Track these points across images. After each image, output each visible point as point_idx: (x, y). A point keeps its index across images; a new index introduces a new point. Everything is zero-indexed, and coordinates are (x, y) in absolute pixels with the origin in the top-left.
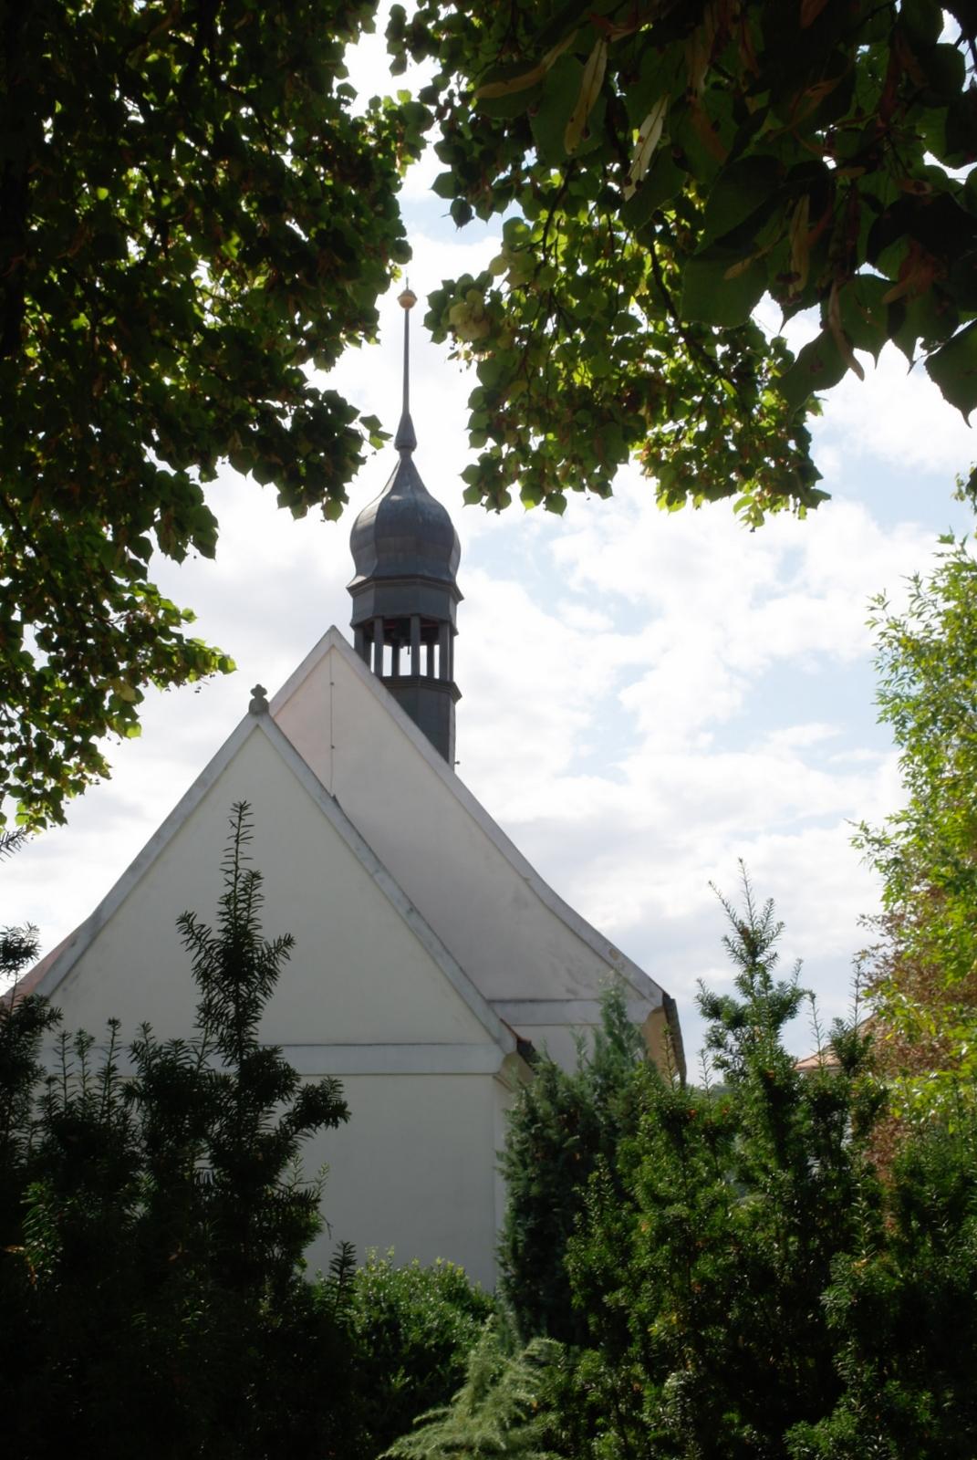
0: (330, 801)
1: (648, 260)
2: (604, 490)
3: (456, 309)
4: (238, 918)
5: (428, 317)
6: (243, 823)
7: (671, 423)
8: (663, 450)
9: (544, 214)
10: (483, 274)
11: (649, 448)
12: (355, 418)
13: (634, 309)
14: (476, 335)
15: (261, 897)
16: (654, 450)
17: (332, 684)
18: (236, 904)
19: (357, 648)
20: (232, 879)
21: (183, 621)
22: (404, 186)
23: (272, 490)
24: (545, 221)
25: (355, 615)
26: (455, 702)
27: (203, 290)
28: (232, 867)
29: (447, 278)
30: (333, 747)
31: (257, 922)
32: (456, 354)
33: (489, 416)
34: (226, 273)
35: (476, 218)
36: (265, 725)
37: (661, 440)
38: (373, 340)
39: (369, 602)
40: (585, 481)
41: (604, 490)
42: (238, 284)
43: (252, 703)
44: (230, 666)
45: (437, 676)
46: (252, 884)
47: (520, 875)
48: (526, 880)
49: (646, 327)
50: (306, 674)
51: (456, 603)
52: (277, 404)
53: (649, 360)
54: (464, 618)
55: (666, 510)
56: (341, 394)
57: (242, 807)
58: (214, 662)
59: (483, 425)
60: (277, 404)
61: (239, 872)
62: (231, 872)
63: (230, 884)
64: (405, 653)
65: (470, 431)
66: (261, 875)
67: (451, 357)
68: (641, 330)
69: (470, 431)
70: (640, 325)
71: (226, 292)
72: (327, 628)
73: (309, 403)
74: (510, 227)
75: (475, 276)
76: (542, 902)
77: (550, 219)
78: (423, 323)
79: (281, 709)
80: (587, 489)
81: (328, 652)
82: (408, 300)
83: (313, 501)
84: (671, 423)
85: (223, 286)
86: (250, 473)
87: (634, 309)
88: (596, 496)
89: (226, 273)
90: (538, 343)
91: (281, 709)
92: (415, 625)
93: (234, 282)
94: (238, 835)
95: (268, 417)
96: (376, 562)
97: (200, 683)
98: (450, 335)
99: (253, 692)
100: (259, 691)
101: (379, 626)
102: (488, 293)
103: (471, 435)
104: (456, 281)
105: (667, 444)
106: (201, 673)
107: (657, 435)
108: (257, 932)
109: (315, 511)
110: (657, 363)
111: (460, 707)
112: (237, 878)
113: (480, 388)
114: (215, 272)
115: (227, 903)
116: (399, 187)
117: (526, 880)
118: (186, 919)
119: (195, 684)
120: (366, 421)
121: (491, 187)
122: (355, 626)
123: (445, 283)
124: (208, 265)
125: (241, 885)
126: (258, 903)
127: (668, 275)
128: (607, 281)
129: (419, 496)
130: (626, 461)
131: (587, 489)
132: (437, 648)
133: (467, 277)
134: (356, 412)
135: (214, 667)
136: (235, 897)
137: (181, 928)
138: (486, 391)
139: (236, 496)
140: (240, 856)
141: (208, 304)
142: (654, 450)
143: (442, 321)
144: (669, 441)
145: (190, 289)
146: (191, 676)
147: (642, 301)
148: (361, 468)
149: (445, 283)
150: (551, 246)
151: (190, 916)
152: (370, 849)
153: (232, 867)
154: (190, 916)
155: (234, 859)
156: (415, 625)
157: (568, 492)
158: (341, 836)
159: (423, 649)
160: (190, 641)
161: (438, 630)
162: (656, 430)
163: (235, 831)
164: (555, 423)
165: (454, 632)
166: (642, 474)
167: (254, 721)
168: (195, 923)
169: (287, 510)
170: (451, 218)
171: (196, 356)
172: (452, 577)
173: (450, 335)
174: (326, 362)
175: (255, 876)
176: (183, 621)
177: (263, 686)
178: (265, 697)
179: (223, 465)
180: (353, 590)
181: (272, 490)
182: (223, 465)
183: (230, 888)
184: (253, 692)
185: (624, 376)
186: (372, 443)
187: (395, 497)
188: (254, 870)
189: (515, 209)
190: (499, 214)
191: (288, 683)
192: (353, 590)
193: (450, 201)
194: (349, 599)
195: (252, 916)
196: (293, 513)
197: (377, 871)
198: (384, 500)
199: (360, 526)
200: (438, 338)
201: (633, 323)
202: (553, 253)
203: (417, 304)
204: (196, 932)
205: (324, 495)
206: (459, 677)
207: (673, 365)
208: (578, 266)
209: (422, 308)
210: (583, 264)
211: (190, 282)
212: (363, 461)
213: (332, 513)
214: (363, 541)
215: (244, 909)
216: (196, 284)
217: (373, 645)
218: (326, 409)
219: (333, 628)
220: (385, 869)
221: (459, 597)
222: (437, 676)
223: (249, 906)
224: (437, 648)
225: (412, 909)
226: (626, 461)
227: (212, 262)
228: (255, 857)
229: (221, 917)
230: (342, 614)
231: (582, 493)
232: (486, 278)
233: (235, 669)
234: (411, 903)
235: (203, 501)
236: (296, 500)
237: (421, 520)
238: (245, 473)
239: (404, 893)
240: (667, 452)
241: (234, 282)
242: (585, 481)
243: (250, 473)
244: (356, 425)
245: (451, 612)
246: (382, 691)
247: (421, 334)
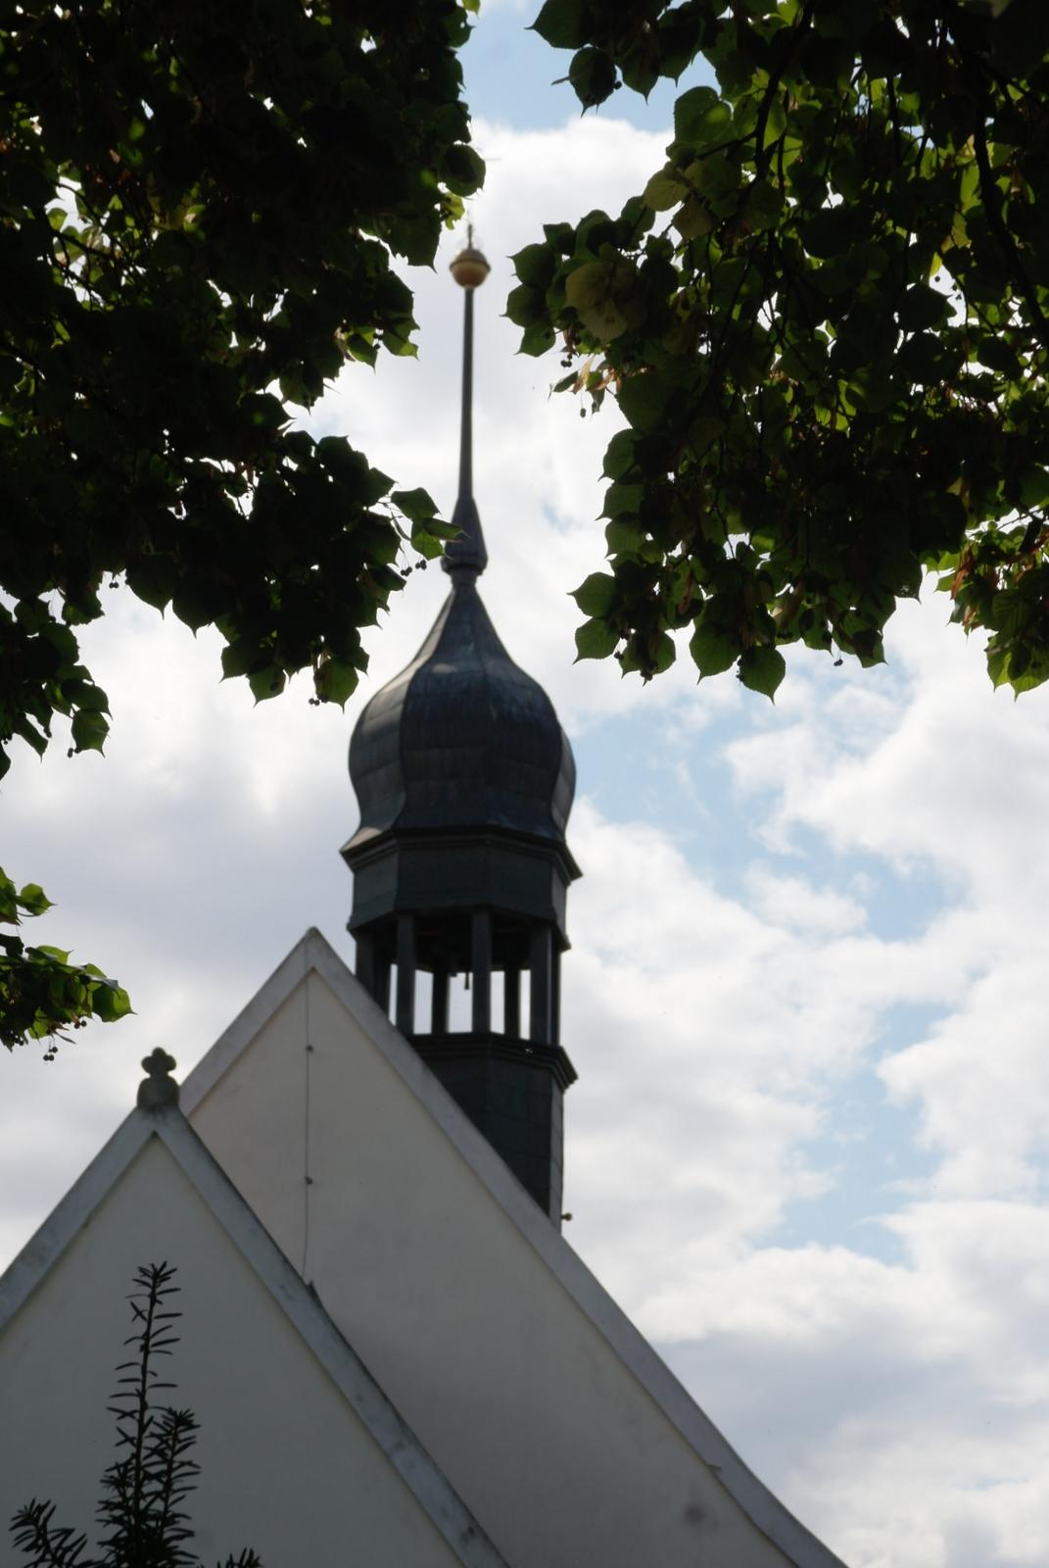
0: (302, 1296)
1: (971, 181)
2: (869, 649)
3: (571, 283)
4: (142, 1516)
5: (514, 297)
6: (158, 1310)
7: (1015, 513)
8: (1000, 570)
9: (761, 79)
10: (634, 205)
11: (970, 565)
12: (383, 493)
13: (942, 281)
14: (617, 330)
15: (194, 1468)
16: (981, 570)
17: (310, 1048)
18: (139, 1485)
19: (361, 974)
20: (131, 1427)
21: (20, 910)
22: (473, 33)
23: (213, 639)
24: (760, 96)
25: (357, 906)
26: (562, 1091)
27: (69, 237)
28: (134, 1404)
29: (556, 220)
30: (309, 1181)
31: (183, 1524)
32: (572, 381)
33: (645, 488)
34: (116, 202)
35: (625, 87)
36: (169, 1133)
37: (996, 548)
38: (405, 348)
39: (388, 882)
40: (830, 627)
41: (869, 649)
42: (138, 226)
43: (144, 1087)
44: (117, 1004)
45: (525, 1033)
46: (176, 1439)
47: (700, 1458)
48: (713, 1470)
49: (960, 317)
50: (254, 1030)
51: (566, 884)
52: (228, 466)
53: (971, 385)
54: (581, 911)
55: (1007, 688)
56: (355, 445)
57: (157, 1277)
58: (85, 995)
59: (634, 508)
60: (228, 466)
61: (147, 1415)
62: (131, 1414)
63: (128, 1439)
64: (460, 992)
65: (607, 521)
66: (196, 1420)
67: (561, 387)
68: (955, 322)
69: (607, 521)
70: (952, 312)
71: (113, 242)
72: (300, 933)
73: (290, 463)
74: (691, 110)
75: (615, 214)
76: (747, 1517)
77: (772, 90)
78: (504, 309)
79: (204, 1099)
80: (834, 645)
81: (304, 981)
82: (471, 270)
83: (295, 666)
84: (1015, 513)
85: (107, 229)
86: (170, 604)
87: (942, 281)
88: (852, 661)
89: (116, 202)
90: (744, 348)
91: (204, 1099)
92: (482, 926)
93: (130, 222)
94: (147, 1336)
95: (210, 491)
96: (402, 799)
97: (55, 1040)
98: (560, 339)
99: (148, 1064)
100: (159, 1063)
101: (406, 930)
102: (643, 244)
103: (609, 527)
104: (574, 227)
105: (1009, 558)
106: (55, 1021)
107: (987, 537)
108: (184, 1545)
109: (302, 682)
110: (983, 389)
111: (572, 1096)
112: (142, 1428)
113: (628, 431)
114: (88, 203)
115: (119, 1483)
116: (463, 35)
117: (713, 1470)
118: (33, 1518)
119: (46, 1041)
120: (401, 499)
121: (654, 24)
122: (356, 929)
123: (549, 229)
124: (77, 186)
125: (150, 1442)
126: (188, 1481)
127: (1011, 205)
128: (882, 221)
129: (491, 665)
130: (913, 592)
131: (834, 645)
132: (525, 977)
133: (597, 216)
134: (388, 483)
135: (85, 1005)
136: (139, 1468)
137: (20, 1539)
138: (637, 438)
139: (143, 650)
140: (150, 1380)
141: (77, 267)
142: (981, 570)
143: (549, 299)
144: (1012, 551)
145: (43, 229)
146: (37, 1025)
147: (954, 263)
148: (393, 597)
149: (549, 229)
150: (772, 148)
151: (41, 1509)
152: (386, 1398)
153: (134, 1404)
154: (41, 1509)
155: (139, 1385)
156: (482, 926)
157: (794, 652)
158: (325, 1372)
159: (497, 979)
160: (35, 953)
161: (531, 939)
162: (984, 527)
163: (140, 1327)
164: (762, 522)
165: (561, 944)
166: (956, 618)
167: (148, 1125)
168: (51, 1525)
169: (243, 681)
170: (568, 89)
171: (62, 369)
172: (560, 832)
173: (560, 339)
174: (307, 391)
175: (183, 1421)
176: (20, 910)
177: (168, 1052)
178: (171, 1074)
179: (115, 593)
180: (351, 855)
181: (213, 639)
182: (115, 593)
183: (128, 1450)
184: (148, 1064)
185: (916, 417)
186: (418, 546)
187: (441, 668)
188: (179, 1409)
189: (701, 72)
190: (671, 81)
191: (218, 1048)
192: (353, 856)
193: (569, 54)
194: (345, 876)
195: (175, 1509)
196: (253, 686)
197: (399, 1446)
198: (418, 673)
199: (369, 726)
200: (535, 344)
201: (940, 307)
202: (773, 167)
203: (490, 279)
204: (54, 1544)
205: (319, 649)
206: (569, 1039)
207: (1015, 394)
208: (825, 195)
209: (502, 282)
210: (835, 191)
211: (42, 219)
212: (398, 583)
213: (333, 687)
214: (370, 755)
215: (157, 1495)
216: (53, 223)
217: (394, 969)
218: (324, 475)
219: (314, 934)
220: (415, 1440)
221: (572, 872)
222: (525, 1033)
223: (168, 1486)
224: (525, 977)
225: (474, 1531)
226: (913, 592)
227: (84, 179)
228: (183, 1379)
229: (105, 1515)
230: (330, 903)
231: (825, 652)
232: (639, 212)
233: (129, 1011)
234: (471, 1517)
235: (77, 658)
236: (259, 662)
237: (494, 714)
238: (161, 606)
239: (455, 1494)
240: (1007, 574)
241: (130, 222)
242: (830, 627)
243: (170, 604)
244: (383, 508)
245: (555, 904)
246: (413, 1064)
247: (499, 333)
